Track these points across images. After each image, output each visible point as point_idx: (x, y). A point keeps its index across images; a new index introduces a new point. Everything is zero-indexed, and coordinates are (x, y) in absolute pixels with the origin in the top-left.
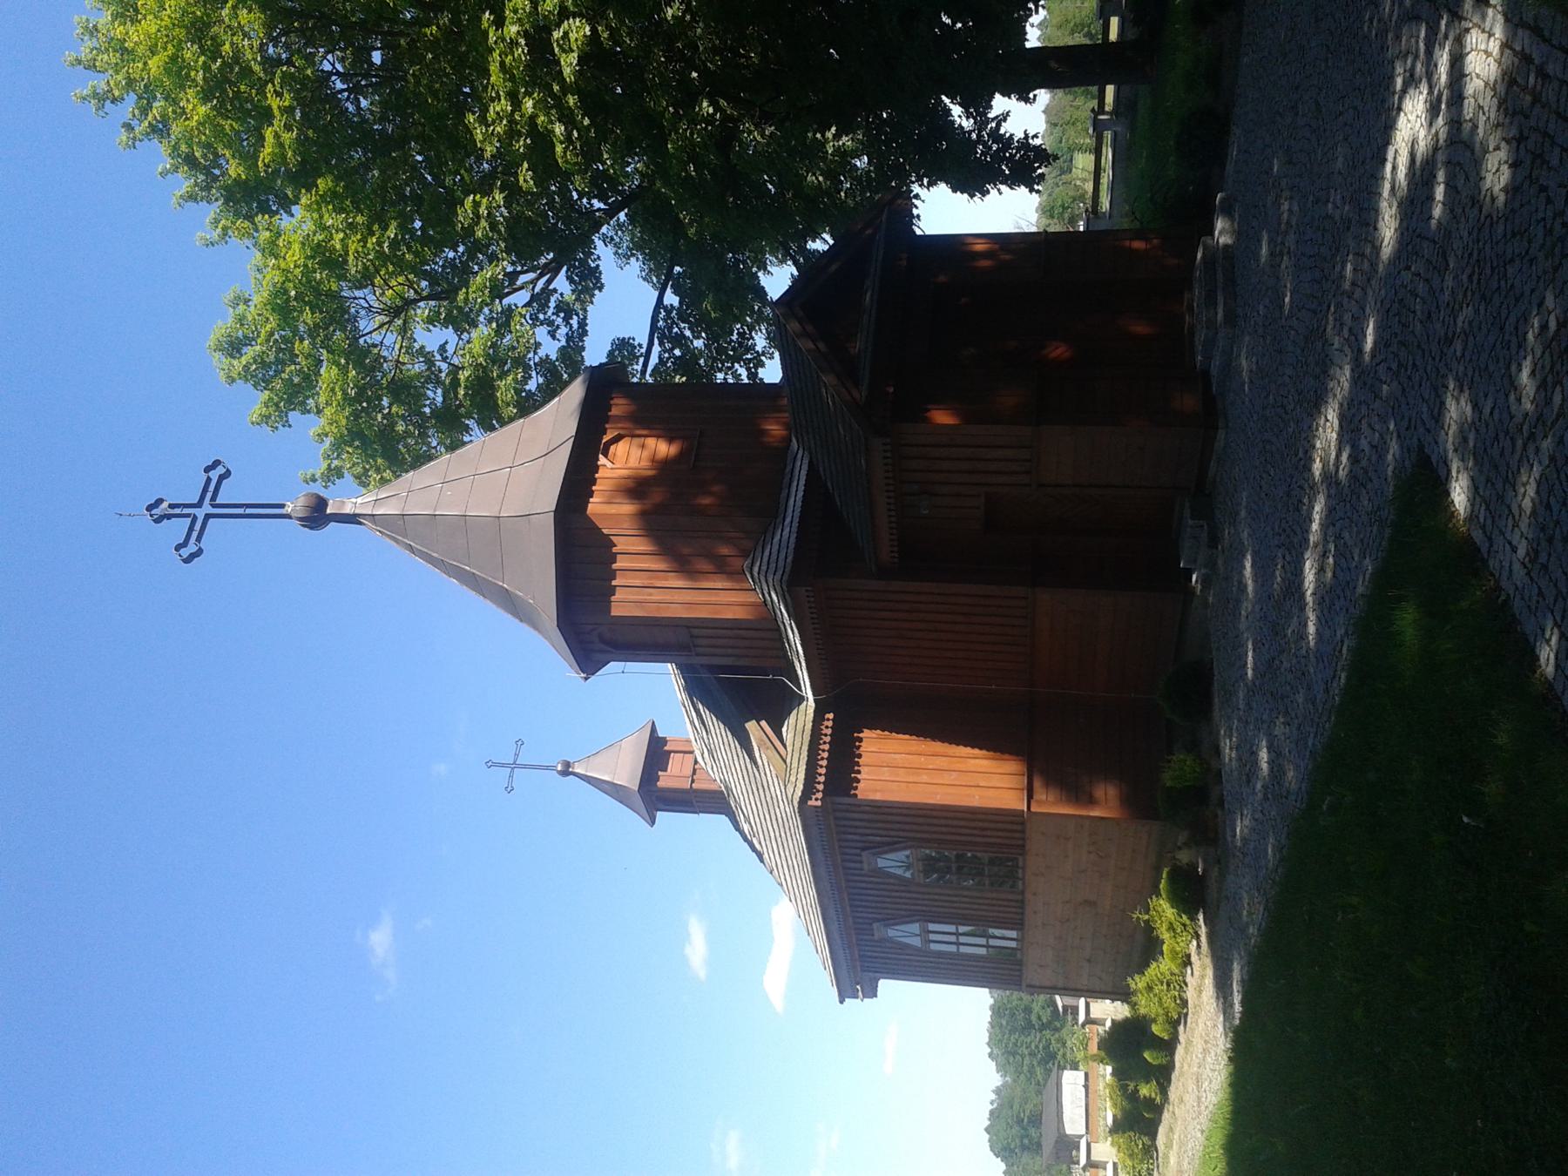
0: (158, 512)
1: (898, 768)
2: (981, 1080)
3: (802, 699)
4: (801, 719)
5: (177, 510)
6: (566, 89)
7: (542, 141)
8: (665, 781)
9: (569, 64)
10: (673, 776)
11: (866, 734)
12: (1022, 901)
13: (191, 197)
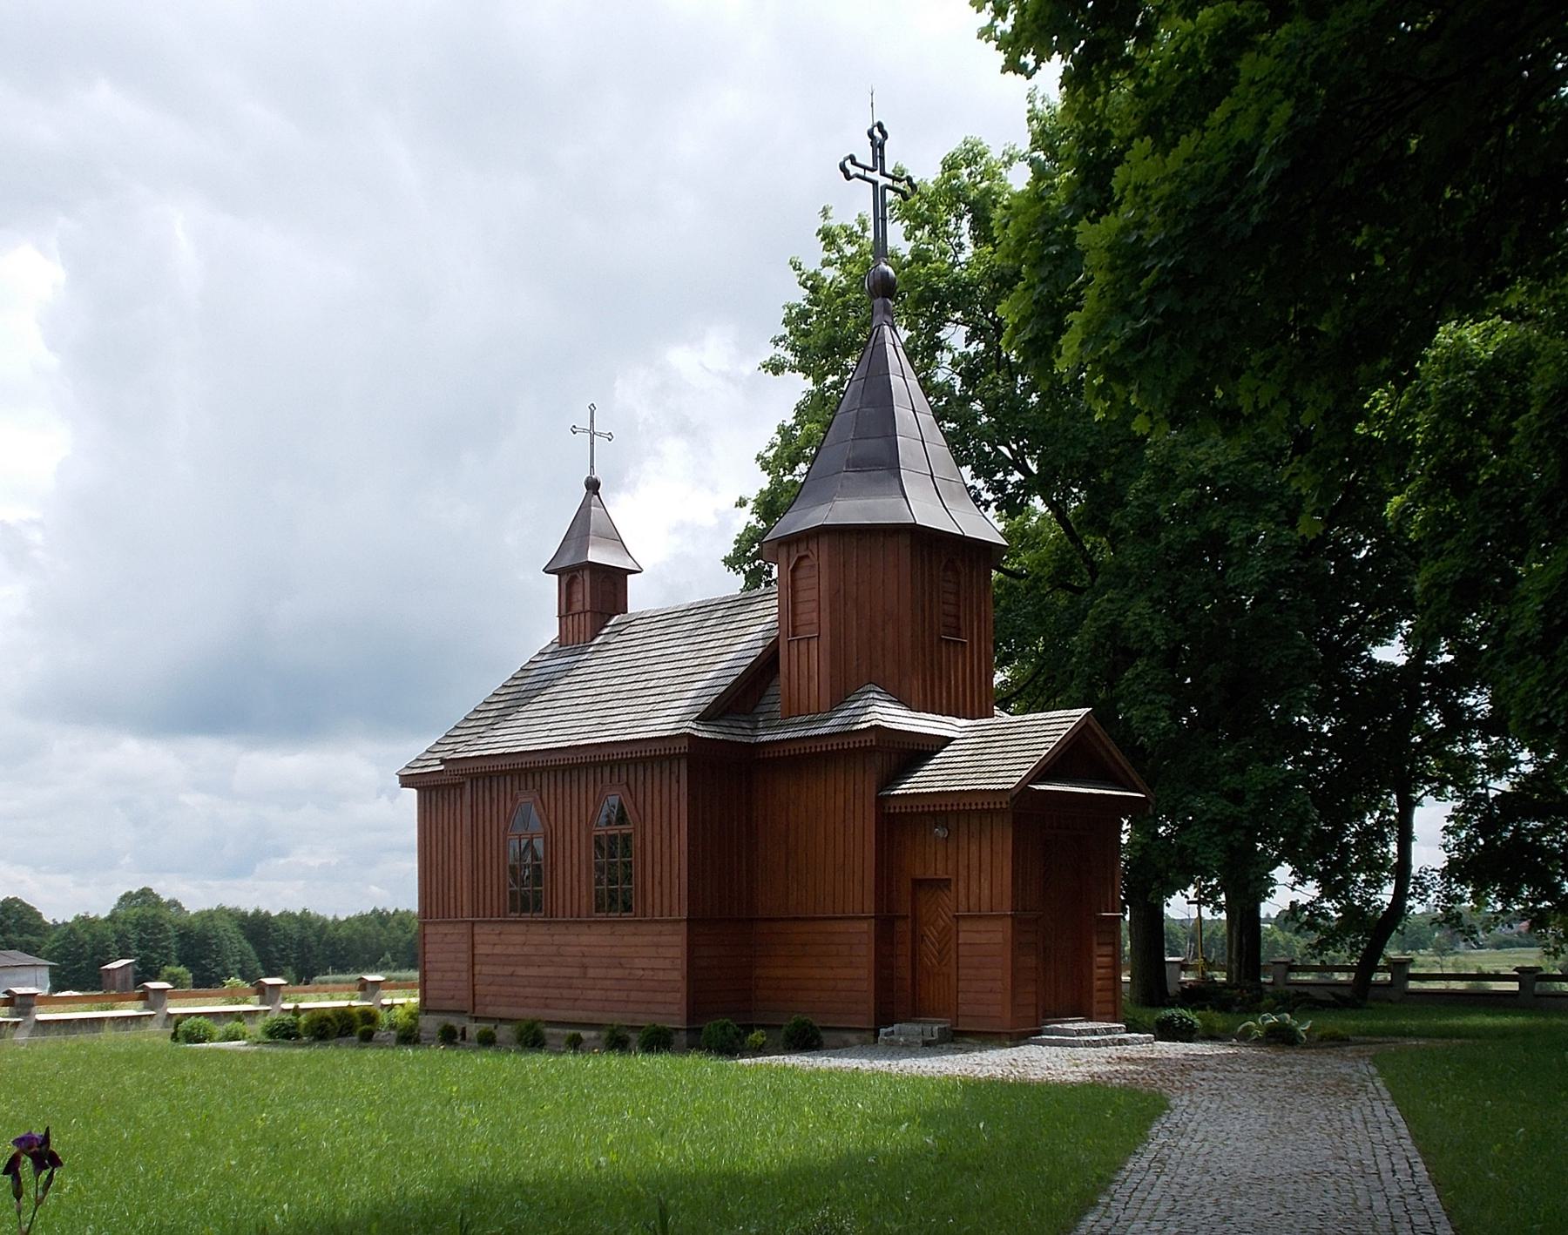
5: (878, 147)
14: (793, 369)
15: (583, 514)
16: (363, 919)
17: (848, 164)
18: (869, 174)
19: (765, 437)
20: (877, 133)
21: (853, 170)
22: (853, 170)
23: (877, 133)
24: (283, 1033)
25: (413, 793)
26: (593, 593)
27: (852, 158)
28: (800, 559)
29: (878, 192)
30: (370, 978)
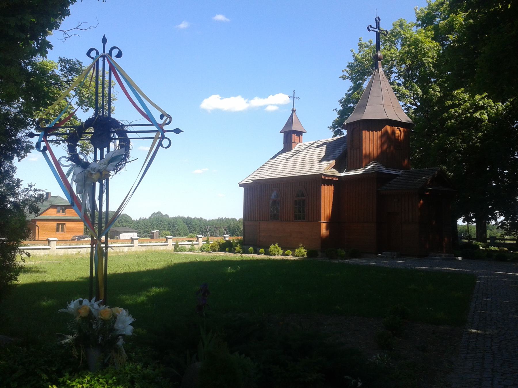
0: (378, 21)
1: (327, 193)
2: (209, 213)
3: (340, 172)
4: (335, 173)
5: (378, 24)
6: (472, 114)
7: (458, 106)
8: (294, 136)
9: (477, 114)
10: (295, 137)
11: (333, 187)
12: (289, 221)
13: (429, 5)
14: (348, 78)
15: (292, 116)
16: (176, 218)
17: (369, 27)
18: (375, 30)
19: (342, 95)
20: (377, 19)
21: (371, 29)
22: (371, 29)
23: (377, 19)
24: (57, 248)
25: (242, 189)
26: (291, 135)
27: (371, 26)
28: (354, 128)
29: (378, 35)
30: (467, 241)
